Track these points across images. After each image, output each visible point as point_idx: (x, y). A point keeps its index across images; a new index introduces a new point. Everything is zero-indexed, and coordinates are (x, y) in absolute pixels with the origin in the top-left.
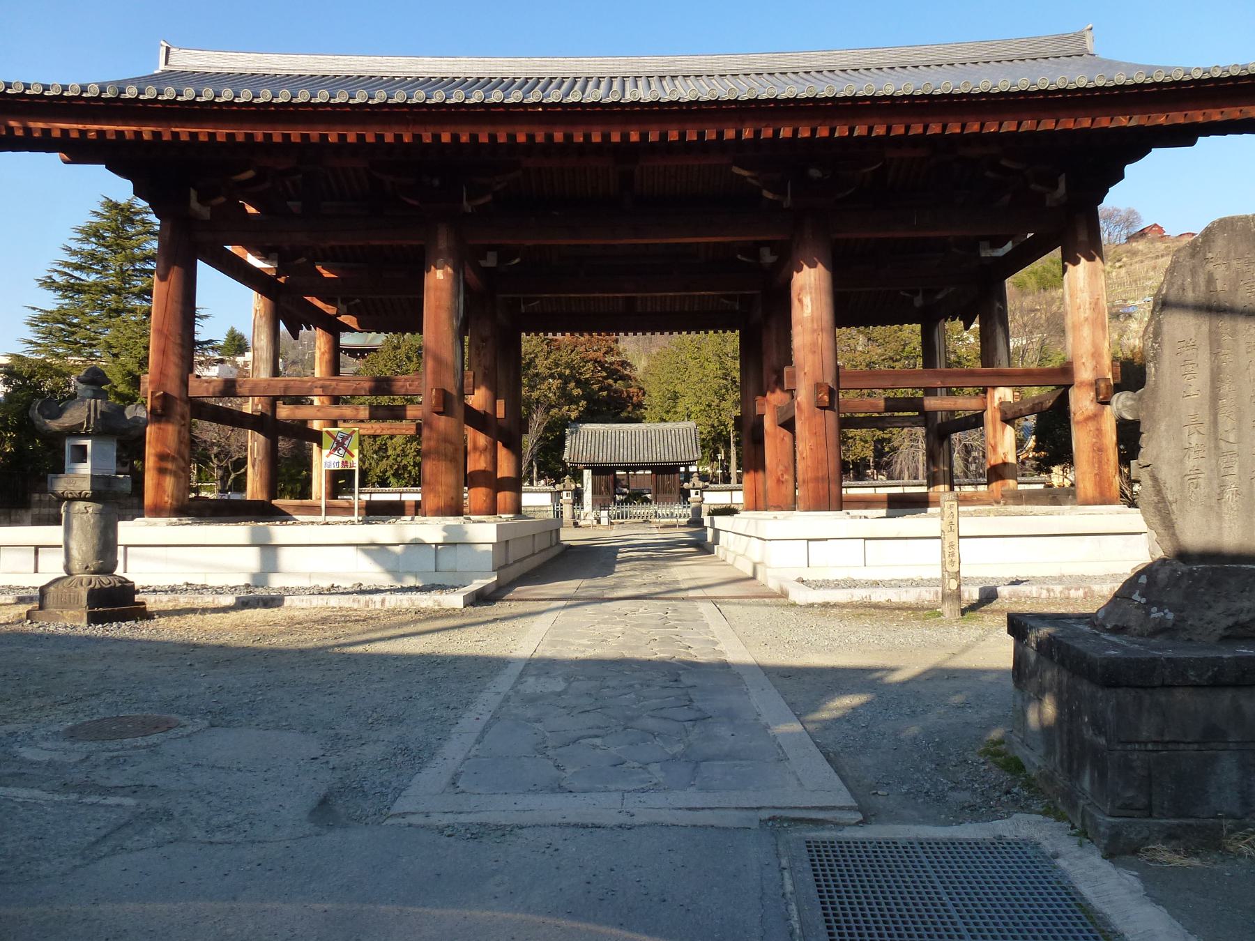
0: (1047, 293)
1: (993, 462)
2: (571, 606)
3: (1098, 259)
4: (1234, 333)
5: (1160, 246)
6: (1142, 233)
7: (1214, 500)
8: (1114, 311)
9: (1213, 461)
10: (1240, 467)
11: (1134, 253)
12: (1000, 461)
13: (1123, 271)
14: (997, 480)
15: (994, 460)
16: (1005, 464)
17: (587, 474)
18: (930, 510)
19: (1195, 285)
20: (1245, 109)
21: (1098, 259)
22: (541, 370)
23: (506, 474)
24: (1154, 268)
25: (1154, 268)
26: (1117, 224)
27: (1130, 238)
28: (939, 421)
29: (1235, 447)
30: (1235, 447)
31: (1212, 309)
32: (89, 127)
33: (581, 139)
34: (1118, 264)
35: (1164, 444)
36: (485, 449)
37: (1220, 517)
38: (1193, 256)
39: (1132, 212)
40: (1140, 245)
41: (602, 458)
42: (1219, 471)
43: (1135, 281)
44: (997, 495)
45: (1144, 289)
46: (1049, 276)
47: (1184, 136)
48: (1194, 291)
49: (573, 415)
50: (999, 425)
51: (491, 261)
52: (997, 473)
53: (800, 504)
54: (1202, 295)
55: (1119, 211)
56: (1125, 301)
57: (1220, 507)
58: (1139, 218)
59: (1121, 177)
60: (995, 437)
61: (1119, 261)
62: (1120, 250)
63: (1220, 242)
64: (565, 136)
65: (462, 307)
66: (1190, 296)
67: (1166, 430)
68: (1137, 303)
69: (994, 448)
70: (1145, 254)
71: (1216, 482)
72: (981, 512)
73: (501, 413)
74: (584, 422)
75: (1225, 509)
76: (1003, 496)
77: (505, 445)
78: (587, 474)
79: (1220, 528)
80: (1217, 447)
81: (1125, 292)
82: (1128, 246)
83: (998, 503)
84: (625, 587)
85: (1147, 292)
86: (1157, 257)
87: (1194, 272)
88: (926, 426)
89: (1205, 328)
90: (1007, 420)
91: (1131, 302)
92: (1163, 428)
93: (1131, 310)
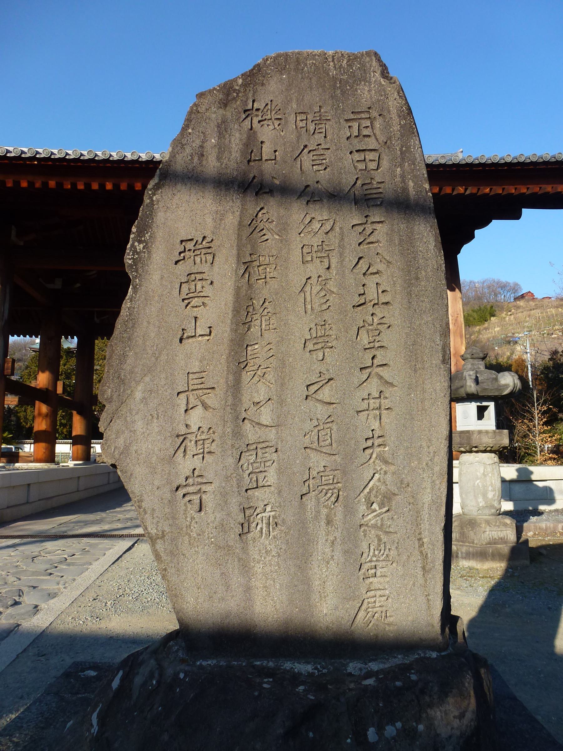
0: (470, 329)
2: (14, 546)
3: (457, 290)
4: (283, 228)
5: (532, 303)
6: (522, 296)
7: (233, 536)
8: (507, 339)
9: (231, 461)
10: (280, 472)
11: (518, 307)
13: (512, 317)
19: (222, 149)
20: (543, 186)
21: (457, 290)
23: (79, 433)
24: (529, 316)
25: (529, 316)
26: (509, 291)
27: (516, 299)
29: (272, 434)
30: (272, 434)
31: (250, 185)
33: (69, 186)
34: (509, 313)
35: (139, 426)
36: (47, 416)
37: (245, 568)
38: (224, 104)
39: (516, 285)
40: (521, 303)
42: (240, 480)
43: (519, 323)
45: (524, 327)
46: (471, 319)
47: (511, 210)
48: (219, 159)
51: (58, 284)
54: (233, 165)
55: (510, 283)
56: (513, 334)
57: (245, 550)
58: (520, 288)
59: (473, 237)
61: (510, 311)
62: (510, 305)
63: (272, 90)
64: (57, 183)
65: (7, 312)
66: (211, 165)
67: (144, 400)
68: (520, 335)
70: (524, 308)
71: (234, 502)
73: (60, 390)
75: (254, 553)
77: (79, 413)
79: (248, 589)
80: (237, 434)
81: (513, 329)
82: (515, 303)
84: (74, 530)
85: (526, 329)
86: (531, 310)
87: (223, 128)
89: (232, 220)
91: (517, 335)
92: (138, 395)
93: (517, 339)
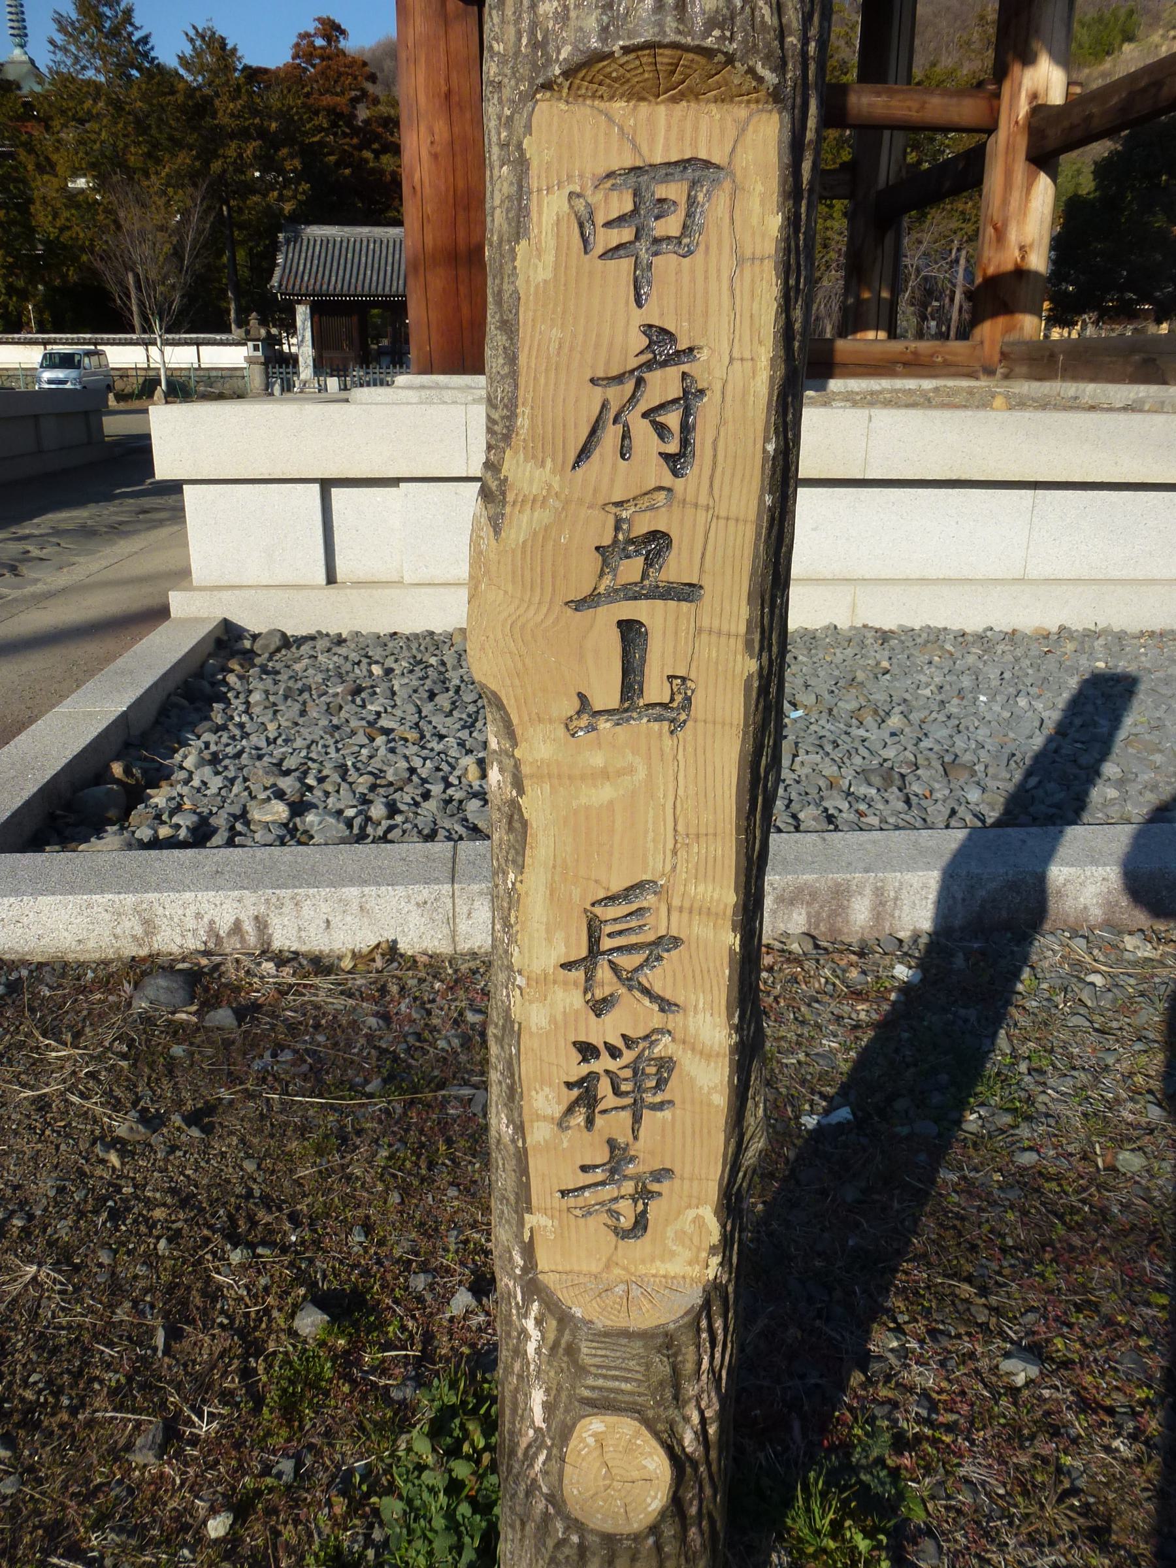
1: (991, 271)
12: (1010, 267)
14: (994, 314)
15: (1000, 261)
16: (1021, 273)
17: (302, 313)
18: (835, 385)
22: (223, 119)
28: (882, 182)
32: (494, 139)
41: (336, 284)
44: (991, 351)
49: (288, 207)
50: (1020, 166)
52: (998, 294)
53: (413, 366)
60: (1005, 202)
69: (1000, 235)
72: (954, 392)
74: (309, 223)
76: (1004, 356)
78: (302, 313)
83: (990, 372)
88: (851, 196)
90: (1043, 158)
